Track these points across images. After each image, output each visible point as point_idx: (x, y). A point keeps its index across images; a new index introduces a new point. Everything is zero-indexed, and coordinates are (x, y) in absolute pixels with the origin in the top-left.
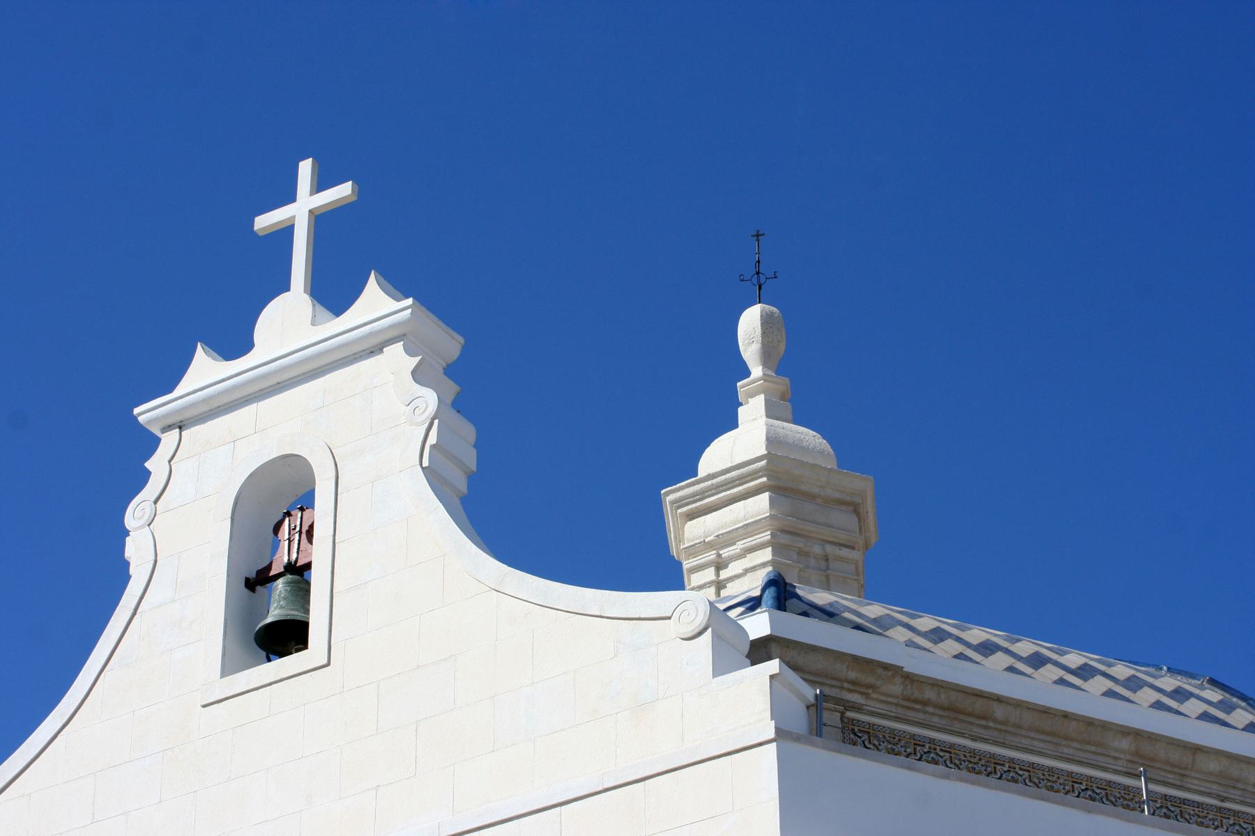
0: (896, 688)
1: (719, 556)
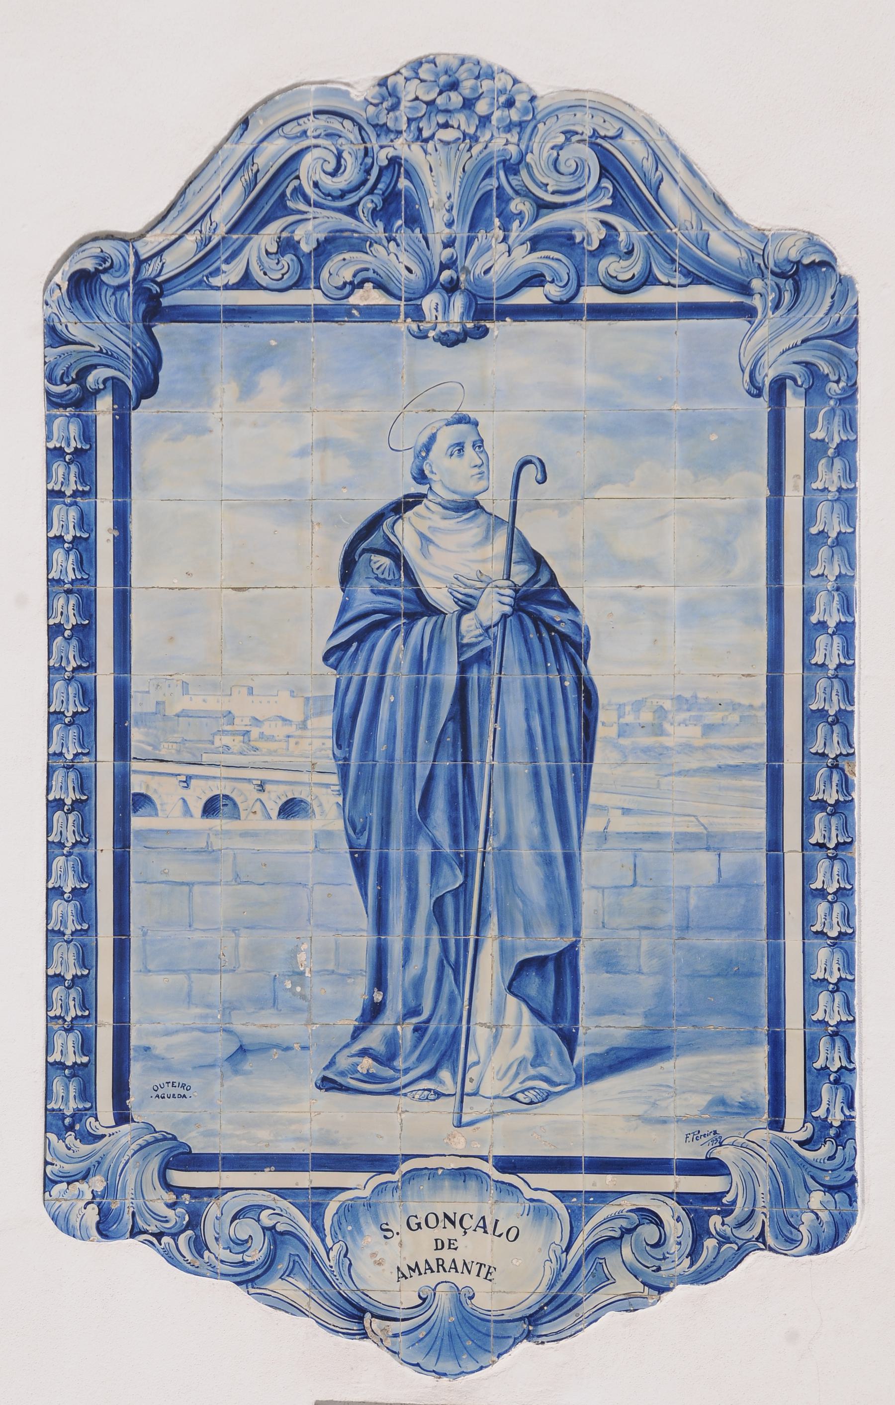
0: (440, 1172)
1: (710, 1235)
